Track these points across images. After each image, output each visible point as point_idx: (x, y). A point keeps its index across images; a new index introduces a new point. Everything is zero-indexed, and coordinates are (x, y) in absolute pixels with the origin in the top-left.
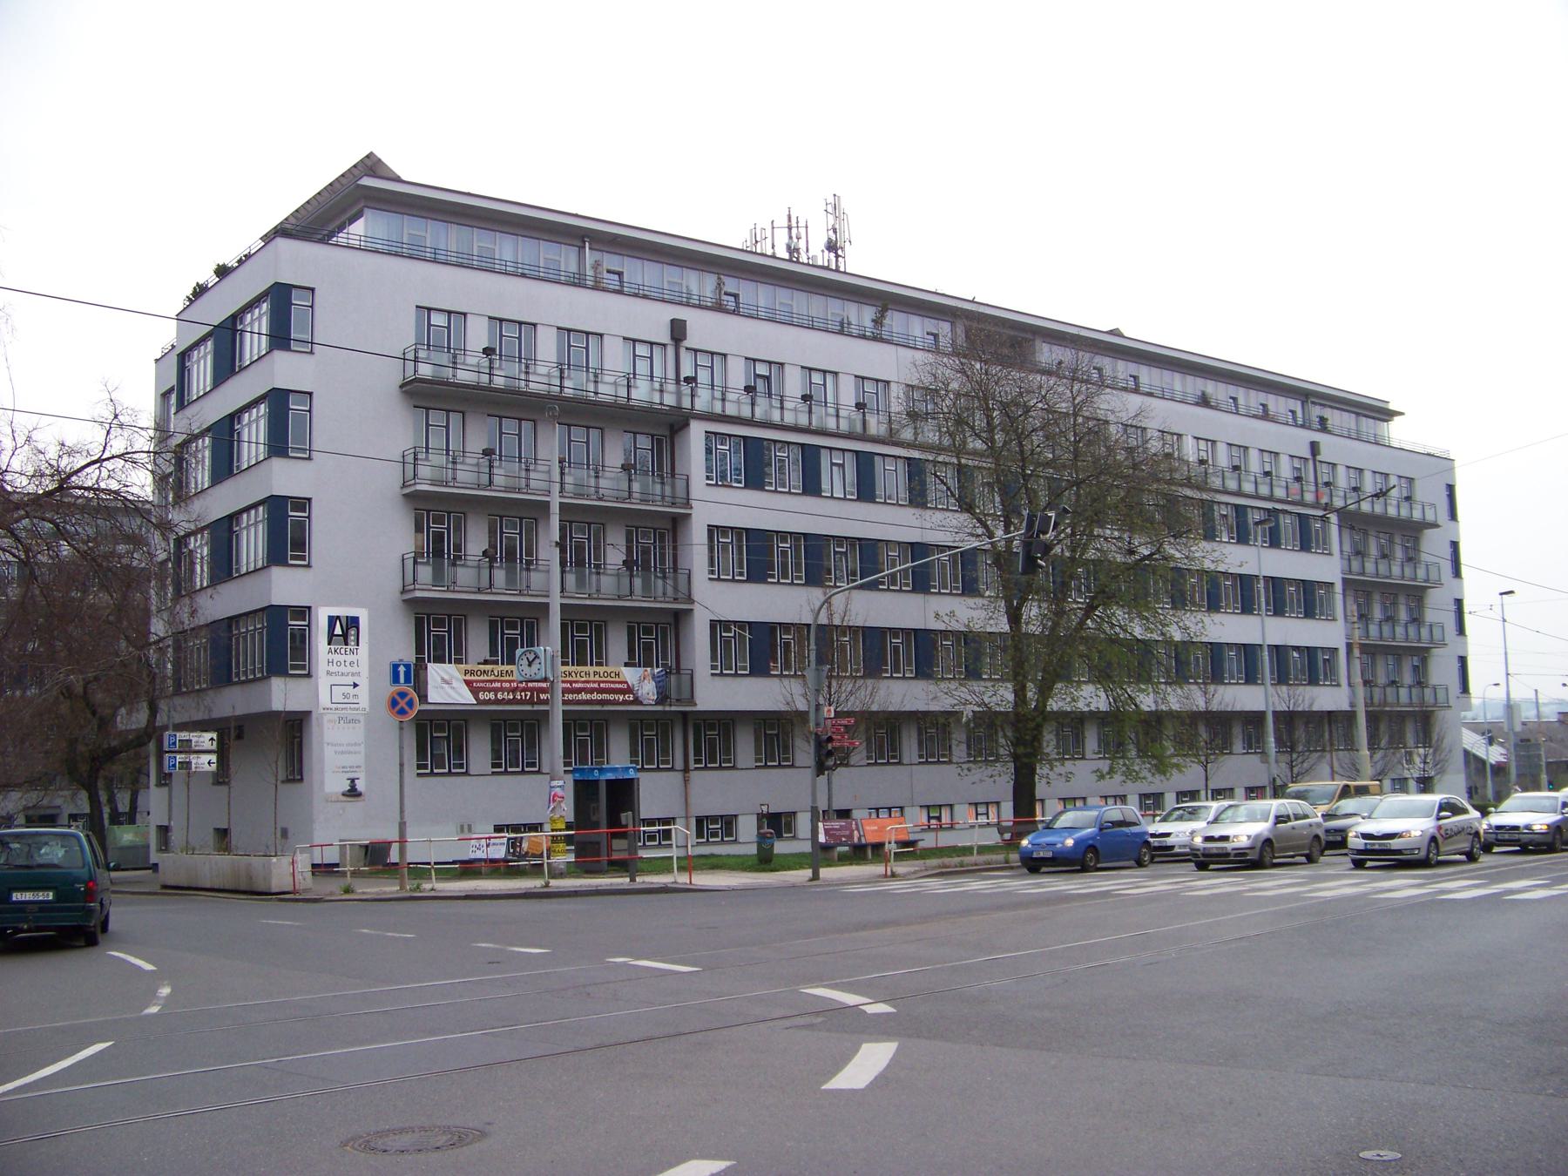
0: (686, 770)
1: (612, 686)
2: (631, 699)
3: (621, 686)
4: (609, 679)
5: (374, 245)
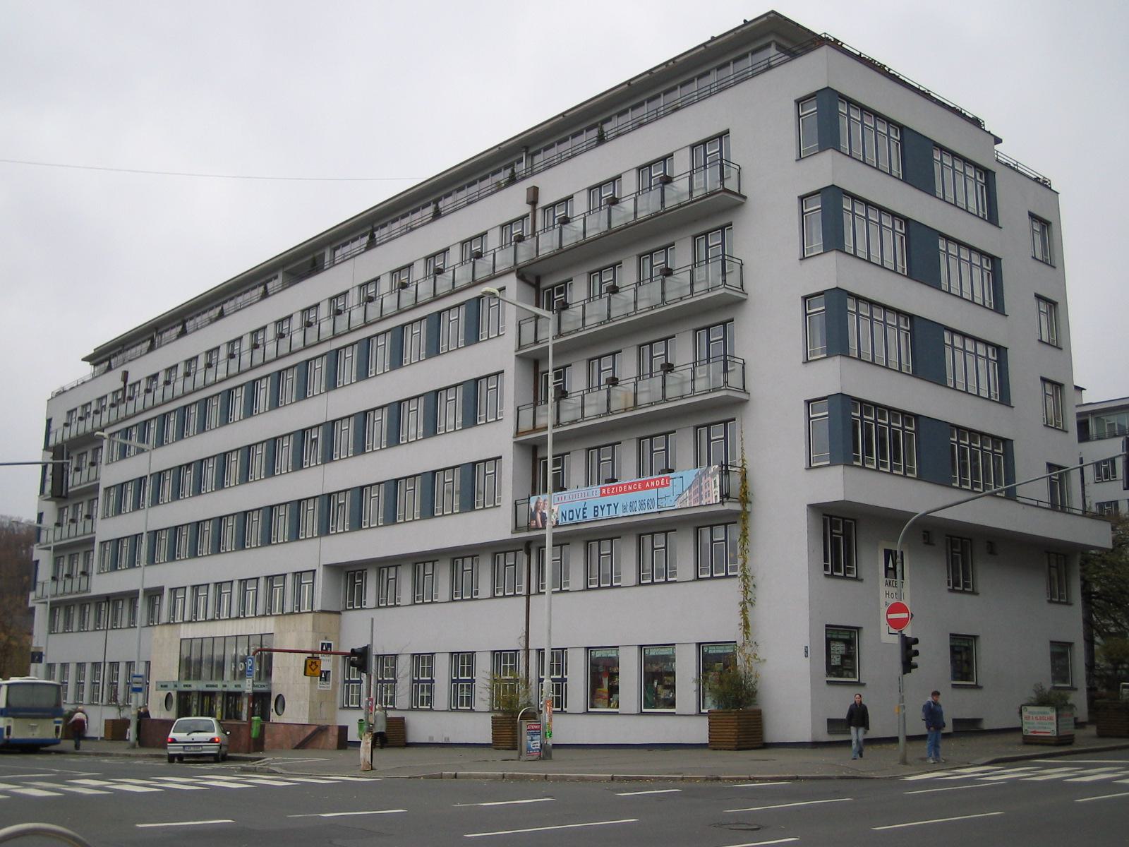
0: (528, 596)
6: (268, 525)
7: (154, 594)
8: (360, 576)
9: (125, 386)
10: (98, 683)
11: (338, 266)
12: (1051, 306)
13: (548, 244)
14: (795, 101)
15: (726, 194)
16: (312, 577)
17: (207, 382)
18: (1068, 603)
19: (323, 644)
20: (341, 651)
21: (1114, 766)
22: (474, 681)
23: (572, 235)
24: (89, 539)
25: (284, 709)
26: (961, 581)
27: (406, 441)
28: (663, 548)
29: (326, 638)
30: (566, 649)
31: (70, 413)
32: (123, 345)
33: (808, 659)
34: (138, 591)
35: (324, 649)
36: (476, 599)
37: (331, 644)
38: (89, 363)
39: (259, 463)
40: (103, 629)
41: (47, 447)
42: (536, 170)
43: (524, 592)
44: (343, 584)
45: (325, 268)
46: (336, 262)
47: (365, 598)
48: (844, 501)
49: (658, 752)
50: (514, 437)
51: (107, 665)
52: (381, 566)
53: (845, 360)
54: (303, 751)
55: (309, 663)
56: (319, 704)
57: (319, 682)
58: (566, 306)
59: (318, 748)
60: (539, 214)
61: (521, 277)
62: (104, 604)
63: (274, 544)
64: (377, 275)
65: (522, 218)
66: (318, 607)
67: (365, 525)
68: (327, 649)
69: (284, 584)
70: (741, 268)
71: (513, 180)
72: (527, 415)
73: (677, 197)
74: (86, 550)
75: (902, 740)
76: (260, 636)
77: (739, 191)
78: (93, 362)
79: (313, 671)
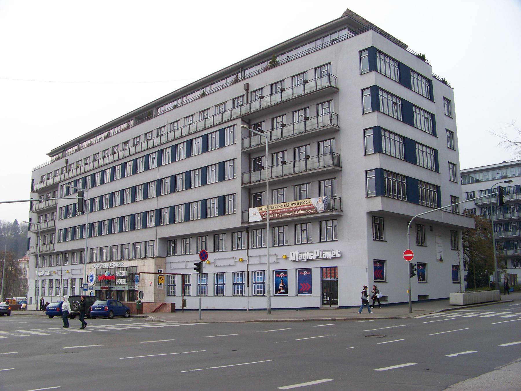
0: (248, 249)
1: (307, 207)
2: (314, 211)
3: (310, 206)
4: (306, 204)
5: (320, 47)
6: (121, 223)
7: (81, 251)
8: (174, 242)
9: (67, 165)
10: (59, 288)
11: (159, 116)
12: (451, 135)
13: (255, 106)
14: (359, 51)
15: (332, 88)
16: (140, 245)
17: (77, 174)
18: (458, 250)
19: (159, 270)
20: (166, 272)
21: (509, 312)
22: (191, 285)
23: (266, 103)
24: (54, 228)
25: (143, 298)
26: (421, 242)
27: (193, 187)
28: (282, 232)
29: (160, 268)
30: (244, 272)
31: (42, 177)
32: (64, 149)
33: (368, 273)
34: (85, 248)
35: (159, 272)
36: (176, 256)
37: (162, 270)
38: (49, 156)
39: (128, 197)
40: (60, 266)
41: (32, 191)
42: (207, 93)
43: (246, 248)
44: (166, 245)
45: (154, 116)
46: (158, 115)
47: (176, 251)
48: (382, 210)
49: (299, 311)
50: (241, 185)
51: (63, 280)
52: (274, 226)
53: (381, 154)
54: (157, 313)
55: (160, 277)
56: (158, 294)
57: (158, 285)
58: (284, 125)
59: (162, 312)
60: (250, 95)
61: (244, 121)
62: (60, 255)
63: (103, 235)
64: (152, 130)
65: (242, 96)
66: (156, 255)
67: (162, 224)
68: (160, 272)
69: (117, 249)
70: (337, 117)
71: (236, 81)
72: (246, 176)
73: (287, 96)
74: (51, 233)
75: (409, 303)
76: (105, 269)
77: (336, 86)
78: (51, 156)
79: (161, 281)
